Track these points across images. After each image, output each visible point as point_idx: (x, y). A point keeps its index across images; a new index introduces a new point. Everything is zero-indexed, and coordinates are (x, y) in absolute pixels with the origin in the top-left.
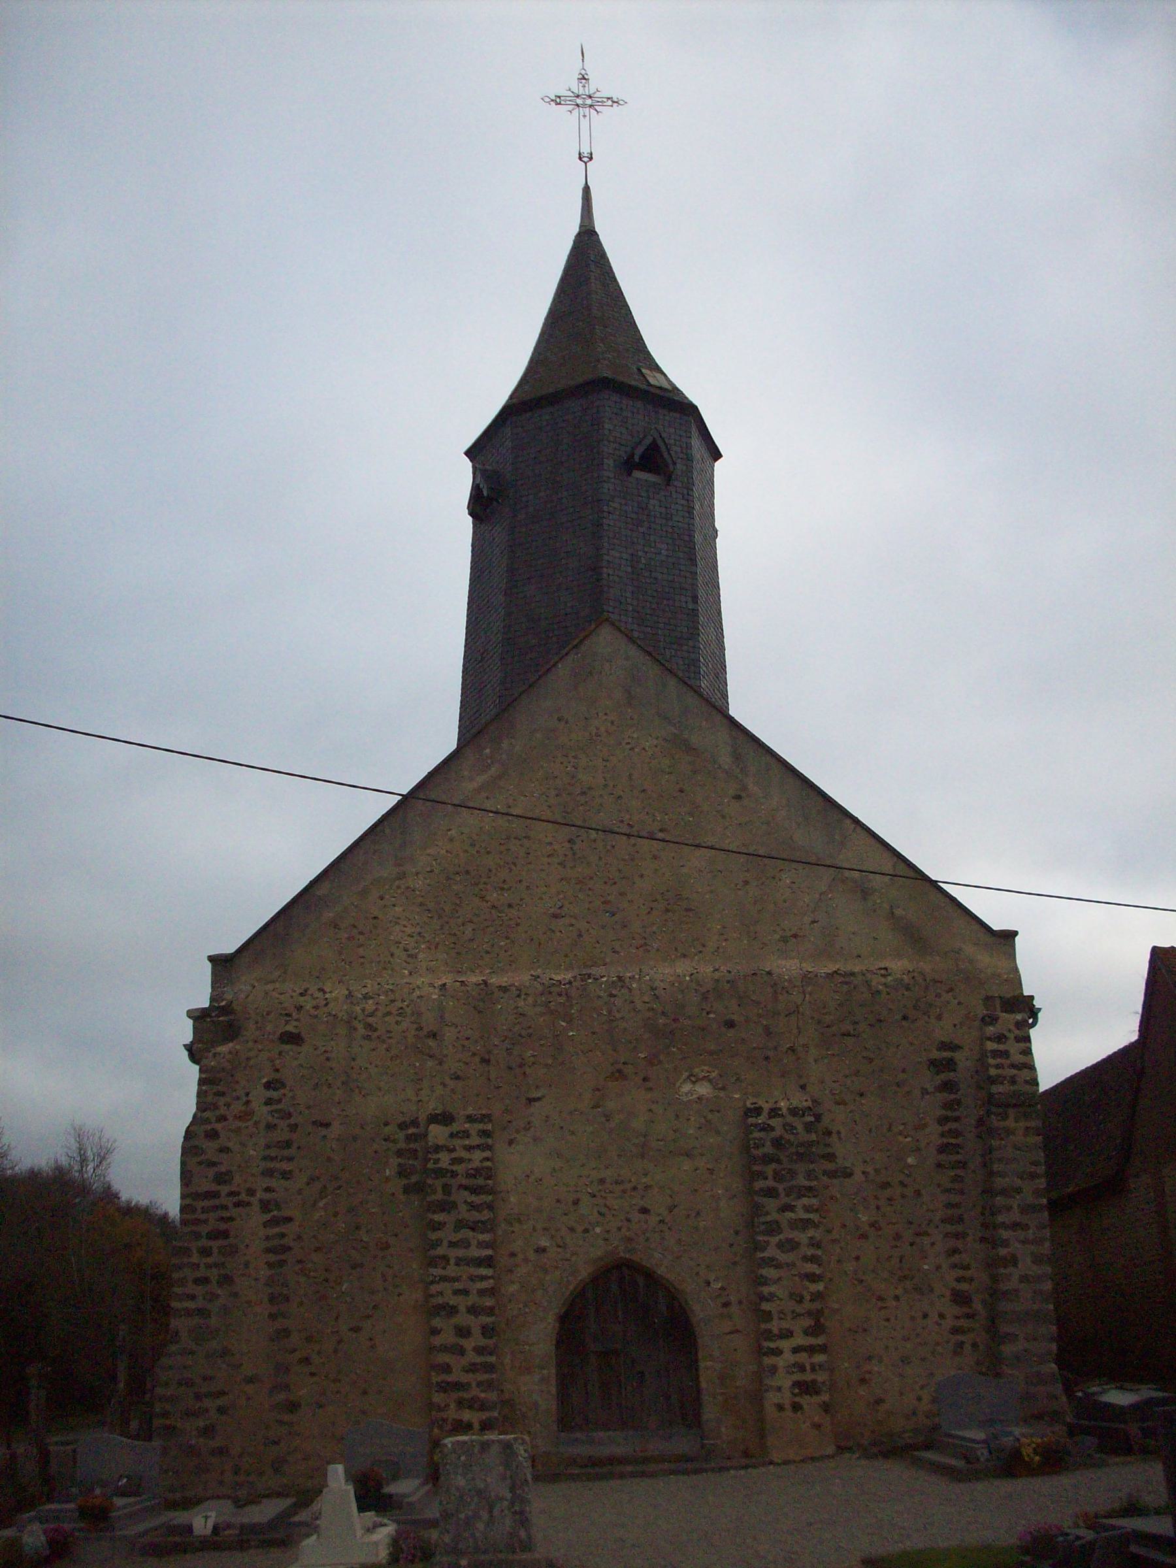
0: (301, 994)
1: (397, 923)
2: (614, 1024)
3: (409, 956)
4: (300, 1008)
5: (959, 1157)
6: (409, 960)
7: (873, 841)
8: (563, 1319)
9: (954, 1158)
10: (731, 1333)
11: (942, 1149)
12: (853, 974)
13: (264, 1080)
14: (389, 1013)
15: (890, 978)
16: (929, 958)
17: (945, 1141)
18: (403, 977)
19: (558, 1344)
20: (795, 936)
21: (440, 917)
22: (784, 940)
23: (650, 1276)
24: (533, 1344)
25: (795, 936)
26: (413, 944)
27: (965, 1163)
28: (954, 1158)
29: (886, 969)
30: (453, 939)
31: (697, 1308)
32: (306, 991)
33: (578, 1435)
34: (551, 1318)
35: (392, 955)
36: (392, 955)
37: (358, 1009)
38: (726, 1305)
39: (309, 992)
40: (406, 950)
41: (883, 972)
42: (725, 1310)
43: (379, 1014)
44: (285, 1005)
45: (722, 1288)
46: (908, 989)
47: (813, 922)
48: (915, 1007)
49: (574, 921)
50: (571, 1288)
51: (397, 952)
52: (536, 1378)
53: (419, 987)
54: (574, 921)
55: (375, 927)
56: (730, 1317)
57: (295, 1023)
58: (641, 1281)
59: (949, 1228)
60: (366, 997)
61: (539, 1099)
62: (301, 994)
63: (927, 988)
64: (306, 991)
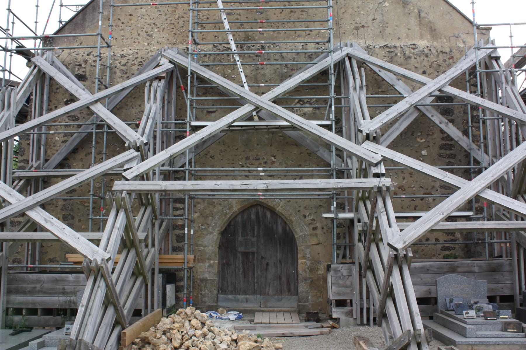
0: (88, 55)
1: (142, 18)
2: (258, 71)
3: (148, 35)
4: (86, 62)
5: (451, 152)
6: (148, 37)
7: (458, 15)
8: (223, 233)
9: (448, 152)
10: (317, 244)
11: (442, 147)
12: (395, 47)
13: (65, 100)
14: (134, 65)
15: (416, 50)
16: (439, 40)
17: (444, 142)
18: (144, 45)
19: (220, 248)
20: (363, 27)
21: (166, 14)
22: (357, 29)
23: (273, 211)
24: (206, 246)
25: (363, 27)
26: (150, 29)
27: (455, 156)
28: (448, 152)
29: (414, 45)
30: (172, 26)
31: (298, 230)
32: (90, 53)
33: (230, 297)
34: (216, 233)
35: (139, 35)
36: (139, 35)
37: (117, 62)
38: (315, 229)
39: (92, 53)
40: (147, 32)
41: (413, 46)
42: (314, 232)
43: (129, 65)
44: (79, 60)
45: (313, 220)
46: (427, 56)
47: (374, 19)
48: (430, 66)
49: (239, 17)
50: (228, 216)
51: (141, 33)
52: (207, 264)
53: (151, 51)
54: (239, 17)
55: (131, 20)
56: (316, 235)
57: (84, 70)
58: (269, 215)
59: (230, 52)
60: (123, 56)
61: (214, 112)
62: (88, 55)
63: (438, 56)
64: (90, 53)
